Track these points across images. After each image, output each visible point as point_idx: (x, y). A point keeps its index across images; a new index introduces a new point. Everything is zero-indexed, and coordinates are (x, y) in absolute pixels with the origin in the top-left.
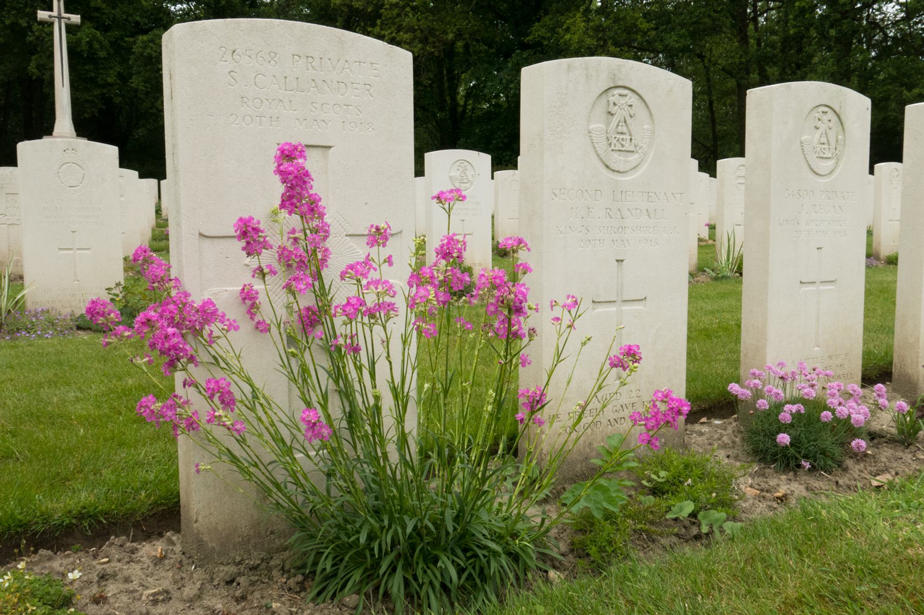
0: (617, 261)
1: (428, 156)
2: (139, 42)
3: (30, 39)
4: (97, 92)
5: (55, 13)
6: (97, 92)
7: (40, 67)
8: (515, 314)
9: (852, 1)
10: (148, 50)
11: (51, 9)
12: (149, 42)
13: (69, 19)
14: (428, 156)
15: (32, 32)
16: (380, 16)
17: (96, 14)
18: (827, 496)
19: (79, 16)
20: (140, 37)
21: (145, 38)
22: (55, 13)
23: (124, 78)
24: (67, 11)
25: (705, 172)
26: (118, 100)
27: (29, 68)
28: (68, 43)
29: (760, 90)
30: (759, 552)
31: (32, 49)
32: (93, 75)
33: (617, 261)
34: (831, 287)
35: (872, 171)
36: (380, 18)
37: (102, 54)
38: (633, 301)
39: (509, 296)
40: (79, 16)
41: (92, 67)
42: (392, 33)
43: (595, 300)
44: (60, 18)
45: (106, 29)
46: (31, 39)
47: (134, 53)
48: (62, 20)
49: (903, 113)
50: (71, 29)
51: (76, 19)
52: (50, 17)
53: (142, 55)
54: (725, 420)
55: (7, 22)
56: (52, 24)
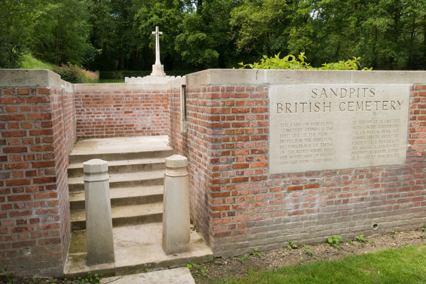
3: (150, 38)
5: (156, 32)
6: (166, 52)
7: (152, 46)
8: (170, 115)
10: (179, 40)
11: (155, 31)
16: (242, 28)
17: (166, 30)
22: (156, 32)
23: (173, 47)
24: (159, 31)
26: (171, 53)
29: (402, 72)
30: (274, 267)
31: (150, 41)
37: (167, 41)
43: (331, 103)
44: (157, 33)
45: (168, 34)
51: (161, 33)
54: (25, 240)
55: (144, 34)
56: (155, 35)
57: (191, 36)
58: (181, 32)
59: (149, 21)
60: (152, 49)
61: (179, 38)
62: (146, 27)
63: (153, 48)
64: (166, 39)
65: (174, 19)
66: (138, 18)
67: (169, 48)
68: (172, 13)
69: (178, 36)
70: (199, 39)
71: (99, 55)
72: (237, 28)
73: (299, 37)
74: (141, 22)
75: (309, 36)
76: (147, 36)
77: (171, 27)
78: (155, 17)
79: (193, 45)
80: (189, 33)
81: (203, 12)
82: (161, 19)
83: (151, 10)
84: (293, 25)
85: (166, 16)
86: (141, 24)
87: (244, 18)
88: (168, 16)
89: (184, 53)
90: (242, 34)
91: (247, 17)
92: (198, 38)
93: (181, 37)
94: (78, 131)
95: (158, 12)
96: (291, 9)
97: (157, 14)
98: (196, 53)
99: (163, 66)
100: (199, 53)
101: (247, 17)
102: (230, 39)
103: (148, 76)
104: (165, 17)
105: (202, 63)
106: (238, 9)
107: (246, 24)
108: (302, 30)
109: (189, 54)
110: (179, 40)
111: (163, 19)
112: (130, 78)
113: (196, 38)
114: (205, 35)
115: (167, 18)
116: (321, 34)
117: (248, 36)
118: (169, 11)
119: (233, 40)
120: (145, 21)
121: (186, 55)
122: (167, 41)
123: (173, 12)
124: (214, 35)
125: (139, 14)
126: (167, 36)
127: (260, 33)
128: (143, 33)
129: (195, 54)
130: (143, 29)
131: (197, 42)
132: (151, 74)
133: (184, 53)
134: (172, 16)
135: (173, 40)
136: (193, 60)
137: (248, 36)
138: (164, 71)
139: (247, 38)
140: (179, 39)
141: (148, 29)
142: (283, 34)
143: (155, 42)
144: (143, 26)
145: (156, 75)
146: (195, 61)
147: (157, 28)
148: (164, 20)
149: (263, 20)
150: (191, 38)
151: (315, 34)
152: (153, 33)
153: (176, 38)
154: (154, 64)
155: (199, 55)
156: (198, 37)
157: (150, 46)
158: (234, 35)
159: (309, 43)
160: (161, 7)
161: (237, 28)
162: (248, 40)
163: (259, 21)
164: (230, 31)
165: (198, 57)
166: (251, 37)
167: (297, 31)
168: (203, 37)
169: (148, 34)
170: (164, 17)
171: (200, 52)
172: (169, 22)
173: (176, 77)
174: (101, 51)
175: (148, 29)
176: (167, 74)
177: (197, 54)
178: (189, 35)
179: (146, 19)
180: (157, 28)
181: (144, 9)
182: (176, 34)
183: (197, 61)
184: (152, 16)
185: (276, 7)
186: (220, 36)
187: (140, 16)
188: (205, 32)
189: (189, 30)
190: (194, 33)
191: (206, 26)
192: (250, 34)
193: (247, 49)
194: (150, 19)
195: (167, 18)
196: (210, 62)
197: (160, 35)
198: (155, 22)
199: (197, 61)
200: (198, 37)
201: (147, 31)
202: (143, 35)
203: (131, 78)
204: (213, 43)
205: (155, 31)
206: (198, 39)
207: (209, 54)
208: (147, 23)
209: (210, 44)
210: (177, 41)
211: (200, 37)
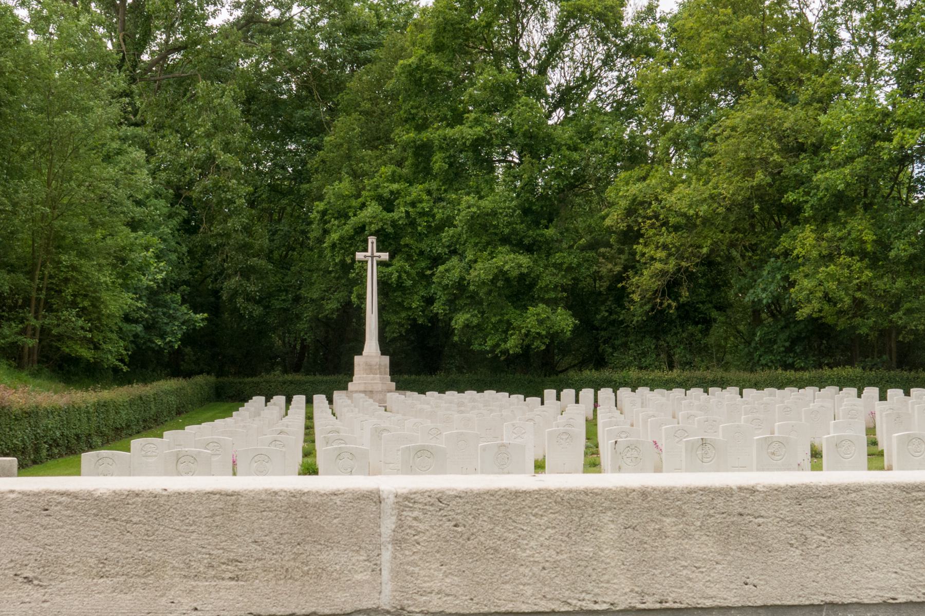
1: (744, 390)
4: (403, 315)
6: (403, 315)
13: (379, 257)
14: (744, 390)
15: (354, 269)
16: (642, 236)
18: (66, 19)
22: (369, 254)
24: (378, 251)
25: (501, 391)
28: (378, 277)
32: (400, 300)
35: (525, 400)
37: (409, 283)
39: (641, 26)
41: (400, 293)
44: (372, 257)
47: (434, 283)
49: (320, 393)
51: (385, 256)
52: (365, 256)
53: (440, 283)
56: (367, 262)
57: (479, 265)
59: (353, 220)
62: (342, 239)
64: (404, 276)
65: (430, 214)
66: (324, 213)
68: (425, 197)
70: (506, 273)
71: (194, 329)
72: (631, 236)
73: (829, 258)
75: (863, 254)
76: (346, 267)
77: (421, 241)
78: (373, 208)
82: (391, 215)
83: (364, 188)
84: (807, 221)
88: (413, 204)
89: (460, 320)
91: (657, 199)
92: (501, 271)
93: (452, 270)
94: (26, 465)
96: (798, 171)
97: (379, 199)
98: (498, 318)
100: (506, 317)
101: (657, 199)
105: (518, 350)
106: (631, 177)
107: (653, 224)
108: (839, 234)
109: (475, 321)
111: (395, 215)
113: (496, 271)
114: (524, 260)
115: (407, 212)
116: (902, 247)
117: (661, 260)
118: (416, 190)
121: (467, 326)
123: (429, 193)
124: (557, 257)
125: (326, 201)
126: (408, 268)
127: (702, 247)
128: (334, 260)
129: (493, 320)
130: (334, 246)
131: (500, 284)
133: (460, 320)
135: (424, 278)
137: (661, 260)
138: (389, 377)
139: (658, 265)
142: (777, 249)
144: (335, 236)
146: (497, 345)
147: (372, 240)
148: (400, 218)
149: (705, 207)
150: (481, 271)
151: (883, 245)
152: (360, 256)
153: (433, 274)
154: (360, 353)
155: (509, 323)
156: (503, 266)
159: (864, 278)
160: (393, 179)
161: (631, 236)
162: (664, 273)
163: (691, 212)
164: (608, 245)
165: (506, 332)
166: (671, 266)
167: (819, 239)
168: (520, 266)
171: (511, 313)
172: (413, 224)
174: (202, 320)
176: (402, 386)
177: (500, 321)
179: (343, 215)
180: (372, 240)
181: (345, 186)
182: (437, 261)
184: (363, 206)
185: (748, 167)
186: (579, 265)
187: (328, 207)
188: (529, 249)
189: (476, 244)
191: (531, 232)
192: (670, 255)
193: (661, 304)
194: (355, 215)
195: (407, 212)
196: (543, 347)
197: (380, 263)
198: (371, 223)
202: (336, 264)
204: (556, 286)
206: (501, 274)
207: (541, 322)
208: (346, 227)
209: (546, 289)
211: (507, 267)
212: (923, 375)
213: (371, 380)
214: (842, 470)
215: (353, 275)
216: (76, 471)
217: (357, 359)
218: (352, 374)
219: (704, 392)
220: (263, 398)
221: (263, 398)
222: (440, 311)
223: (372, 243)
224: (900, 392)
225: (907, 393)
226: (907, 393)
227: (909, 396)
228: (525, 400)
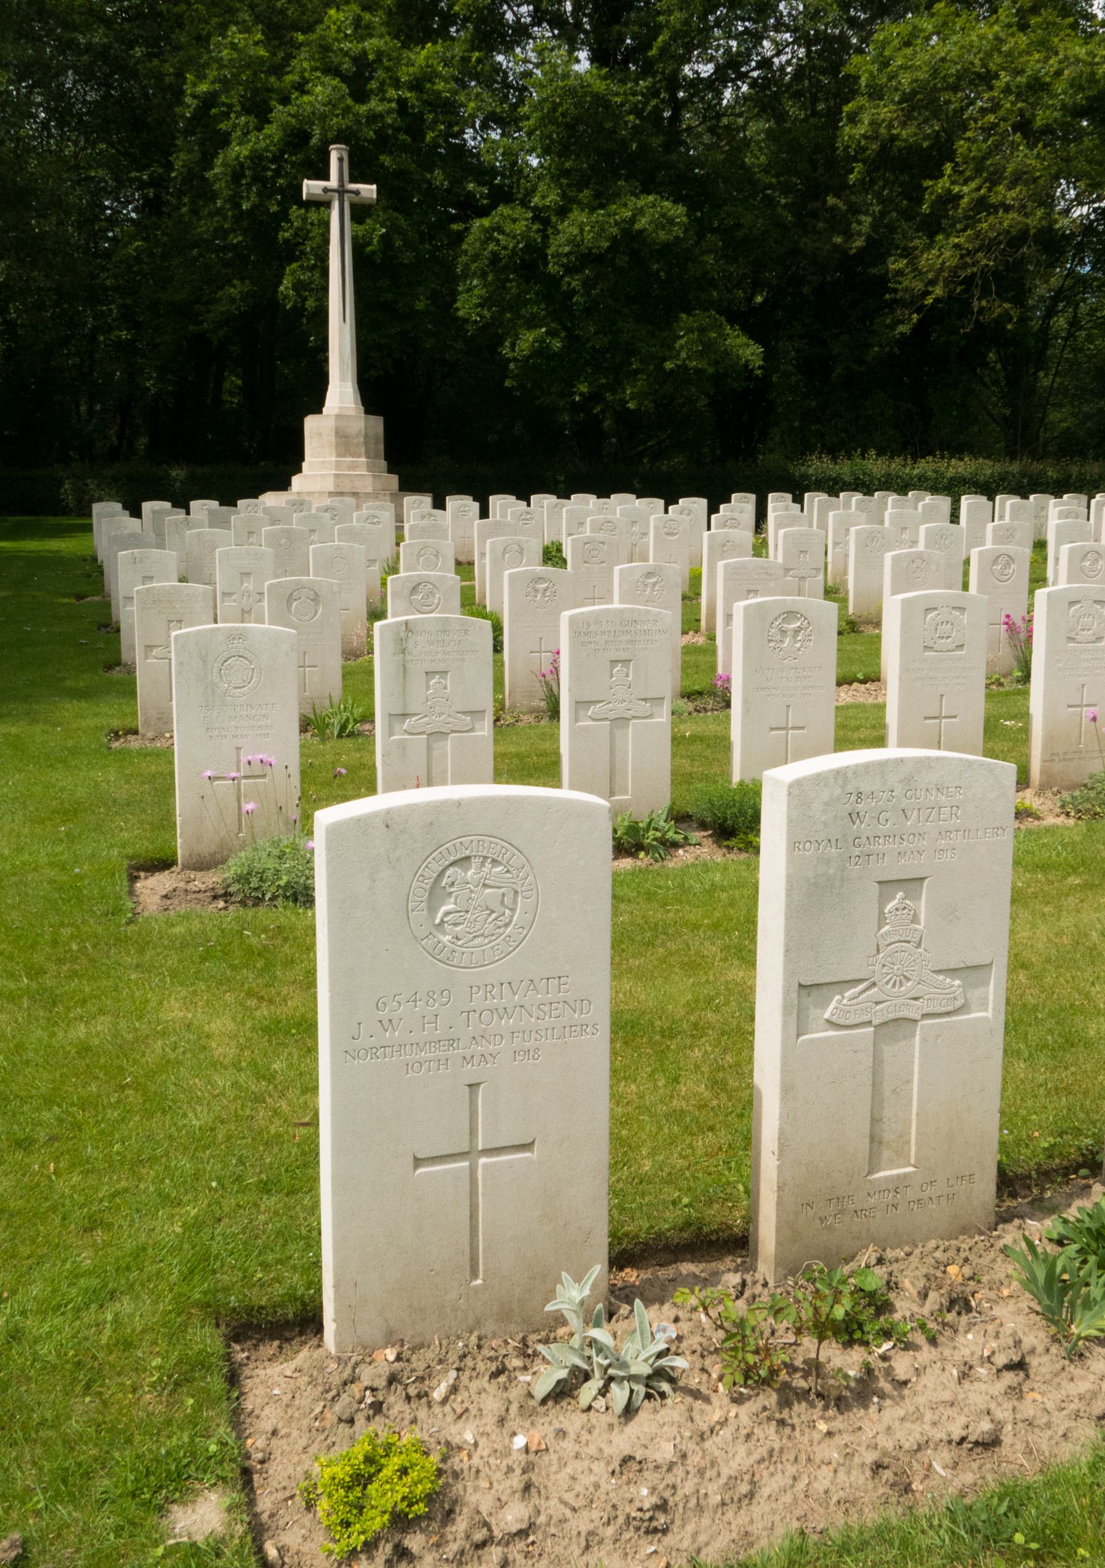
0: (879, 883)
2: (474, 230)
5: (333, 182)
9: (493, 2)
10: (492, 246)
11: (327, 178)
12: (494, 229)
15: (289, 221)
19: (374, 187)
20: (477, 223)
21: (486, 222)
22: (333, 182)
23: (445, 303)
24: (353, 179)
25: (91, 511)
27: (282, 288)
31: (290, 252)
32: (389, 296)
33: (879, 883)
34: (527, 1155)
35: (666, 511)
36: (952, 160)
38: (432, 1158)
40: (374, 187)
42: (979, 189)
44: (341, 191)
46: (287, 235)
48: (346, 196)
50: (360, 212)
51: (369, 191)
57: (578, 216)
58: (501, 196)
60: (299, 311)
61: (488, 236)
62: (256, 158)
63: (310, 304)
67: (420, 305)
69: (480, 224)
74: (223, 126)
79: (587, 284)
80: (564, 196)
81: (663, 50)
85: (397, 84)
86: (224, 141)
87: (987, 79)
88: (417, 85)
90: (959, 196)
95: (347, 66)
99: (377, 423)
102: (836, 247)
103: (270, 499)
104: (392, 93)
110: (492, 246)
112: (834, 499)
115: (402, 103)
119: (861, 250)
120: (253, 120)
121: (541, 351)
122: (407, 257)
128: (238, 206)
130: (236, 175)
131: (622, 261)
132: (295, 480)
134: (440, 86)
136: (583, 388)
138: (383, 464)
140: (491, 238)
141: (277, 173)
143: (324, 258)
144: (238, 151)
145: (330, 486)
146: (594, 397)
152: (311, 187)
153: (467, 229)
154: (317, 407)
156: (633, 220)
157: (286, 286)
158: (867, 220)
164: (841, 189)
169: (274, 208)
170: (382, 90)
173: (713, 509)
175: (277, 173)
178: (563, 212)
179: (260, 111)
183: (609, 397)
187: (217, 86)
190: (597, 195)
195: (402, 103)
199: (609, 397)
200: (633, 220)
201: (267, 190)
203: (235, 505)
205: (327, 178)
207: (708, 348)
210: (476, 258)
212: (1093, 469)
213: (350, 468)
214: (1046, 677)
215: (287, 235)
216: (132, 628)
217: (311, 423)
218: (301, 457)
219: (794, 501)
220: (702, 503)
221: (702, 503)
222: (474, 317)
223: (341, 160)
224: (427, 500)
225: (439, 504)
226: (439, 504)
227: (444, 509)
228: (666, 511)
